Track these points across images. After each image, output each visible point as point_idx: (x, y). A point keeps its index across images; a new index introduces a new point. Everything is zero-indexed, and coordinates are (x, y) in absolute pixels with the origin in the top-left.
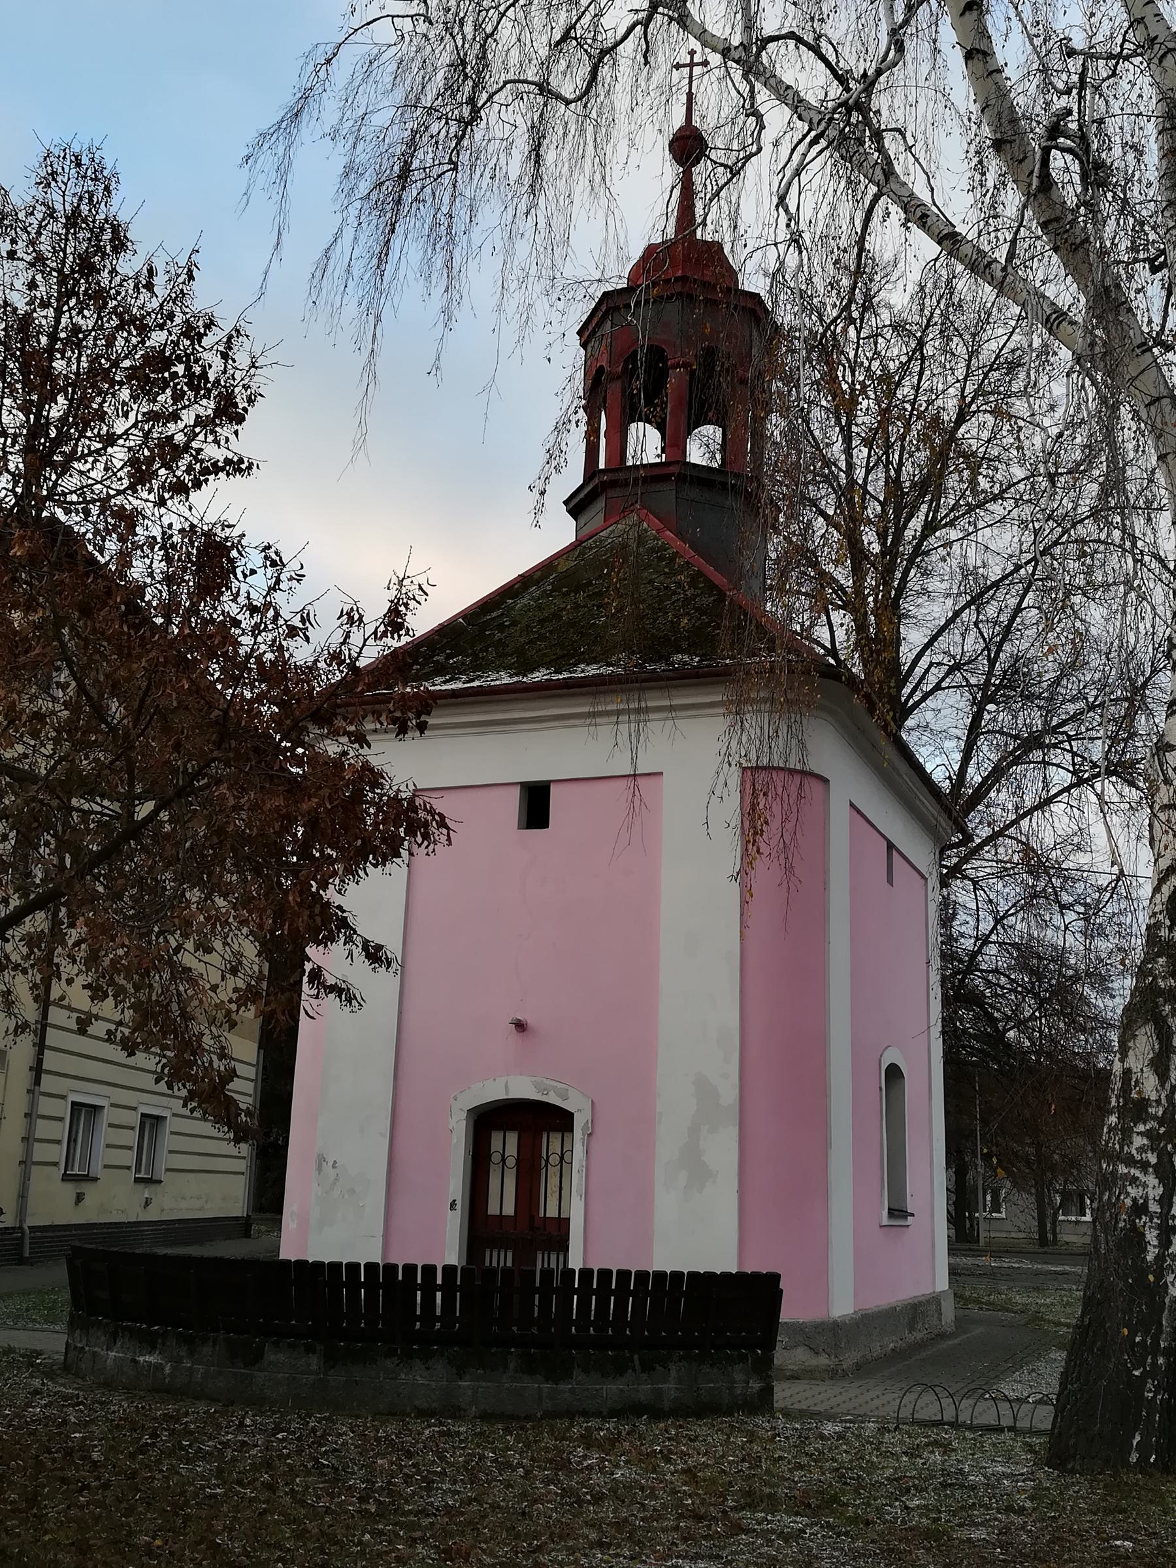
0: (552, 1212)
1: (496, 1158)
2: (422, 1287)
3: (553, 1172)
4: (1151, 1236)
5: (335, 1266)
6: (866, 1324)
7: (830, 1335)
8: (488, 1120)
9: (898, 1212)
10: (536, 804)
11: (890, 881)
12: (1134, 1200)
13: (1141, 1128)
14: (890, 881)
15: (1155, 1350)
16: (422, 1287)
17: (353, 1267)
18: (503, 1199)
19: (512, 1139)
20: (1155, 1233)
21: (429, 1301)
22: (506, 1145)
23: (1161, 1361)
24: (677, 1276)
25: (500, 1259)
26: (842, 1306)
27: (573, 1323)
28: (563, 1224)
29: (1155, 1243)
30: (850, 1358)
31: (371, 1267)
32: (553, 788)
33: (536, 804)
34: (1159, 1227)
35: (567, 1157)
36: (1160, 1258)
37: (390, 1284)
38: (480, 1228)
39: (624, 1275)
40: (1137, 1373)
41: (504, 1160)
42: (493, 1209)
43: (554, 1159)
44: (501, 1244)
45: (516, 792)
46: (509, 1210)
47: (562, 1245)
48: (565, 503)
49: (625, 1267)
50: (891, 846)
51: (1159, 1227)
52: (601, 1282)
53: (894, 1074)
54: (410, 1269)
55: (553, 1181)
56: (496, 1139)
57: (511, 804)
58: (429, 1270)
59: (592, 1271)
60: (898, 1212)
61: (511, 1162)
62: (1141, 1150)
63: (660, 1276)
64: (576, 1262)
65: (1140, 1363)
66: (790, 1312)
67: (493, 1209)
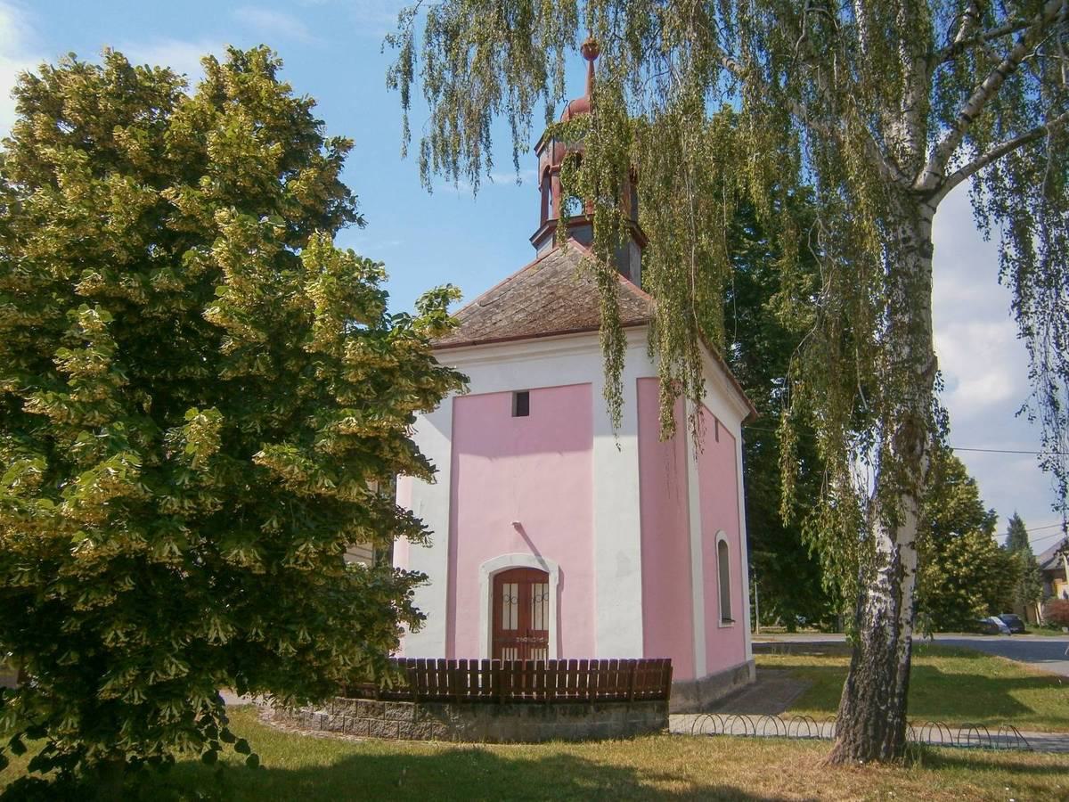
0: (539, 627)
1: (506, 598)
2: (482, 672)
3: (539, 605)
4: (889, 630)
5: (421, 662)
6: (716, 680)
7: (695, 688)
8: (500, 579)
9: (726, 619)
10: (522, 403)
11: (717, 439)
12: (879, 611)
13: (882, 569)
14: (717, 439)
15: (893, 694)
16: (482, 672)
17: (431, 662)
18: (511, 621)
19: (515, 587)
20: (891, 628)
21: (474, 679)
22: (511, 591)
23: (896, 700)
24: (614, 662)
25: (510, 655)
26: (701, 672)
27: (556, 689)
28: (545, 634)
29: (892, 633)
30: (706, 700)
31: (441, 662)
32: (531, 395)
33: (522, 403)
34: (894, 625)
35: (546, 597)
36: (895, 642)
37: (453, 671)
38: (500, 638)
39: (584, 663)
40: (883, 708)
41: (510, 599)
42: (505, 626)
43: (539, 599)
44: (512, 645)
45: (511, 395)
46: (515, 626)
47: (545, 645)
48: (531, 240)
49: (604, 658)
50: (717, 421)
51: (894, 625)
52: (560, 667)
53: (722, 544)
54: (463, 663)
55: (539, 611)
56: (506, 587)
57: (508, 404)
58: (474, 663)
59: (566, 661)
60: (726, 619)
61: (515, 601)
62: (883, 582)
63: (604, 663)
64: (553, 656)
65: (884, 702)
66: (678, 676)
67: (505, 626)
